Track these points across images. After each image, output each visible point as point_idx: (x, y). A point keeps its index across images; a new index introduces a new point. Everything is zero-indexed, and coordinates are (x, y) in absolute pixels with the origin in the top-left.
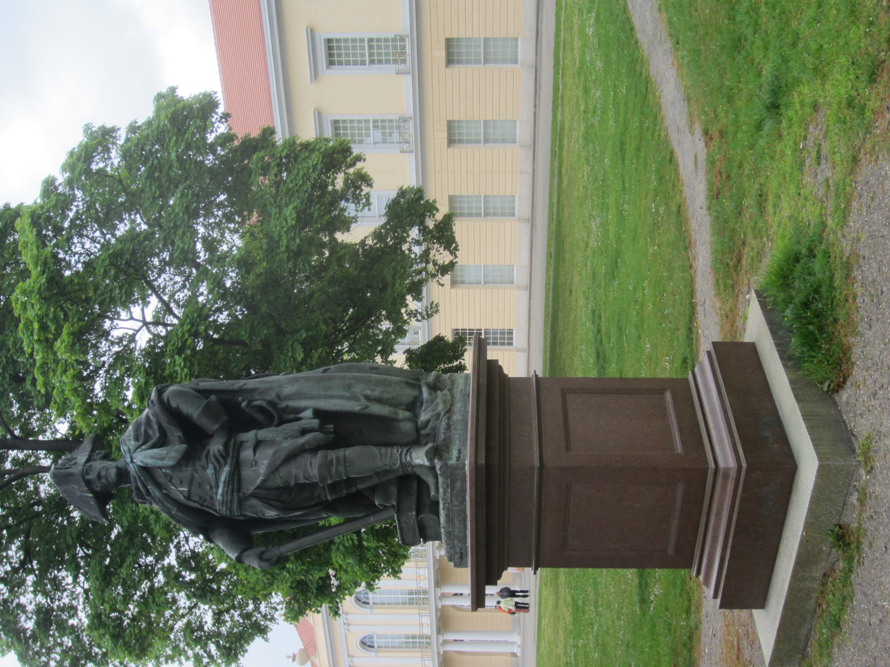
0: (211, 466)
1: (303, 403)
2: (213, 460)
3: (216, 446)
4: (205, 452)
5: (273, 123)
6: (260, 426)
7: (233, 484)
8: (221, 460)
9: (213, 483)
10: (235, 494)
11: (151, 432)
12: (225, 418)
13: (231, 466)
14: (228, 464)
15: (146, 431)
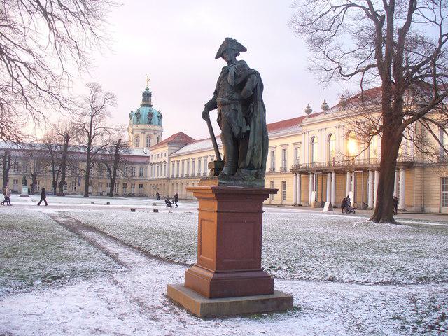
3: (235, 96)
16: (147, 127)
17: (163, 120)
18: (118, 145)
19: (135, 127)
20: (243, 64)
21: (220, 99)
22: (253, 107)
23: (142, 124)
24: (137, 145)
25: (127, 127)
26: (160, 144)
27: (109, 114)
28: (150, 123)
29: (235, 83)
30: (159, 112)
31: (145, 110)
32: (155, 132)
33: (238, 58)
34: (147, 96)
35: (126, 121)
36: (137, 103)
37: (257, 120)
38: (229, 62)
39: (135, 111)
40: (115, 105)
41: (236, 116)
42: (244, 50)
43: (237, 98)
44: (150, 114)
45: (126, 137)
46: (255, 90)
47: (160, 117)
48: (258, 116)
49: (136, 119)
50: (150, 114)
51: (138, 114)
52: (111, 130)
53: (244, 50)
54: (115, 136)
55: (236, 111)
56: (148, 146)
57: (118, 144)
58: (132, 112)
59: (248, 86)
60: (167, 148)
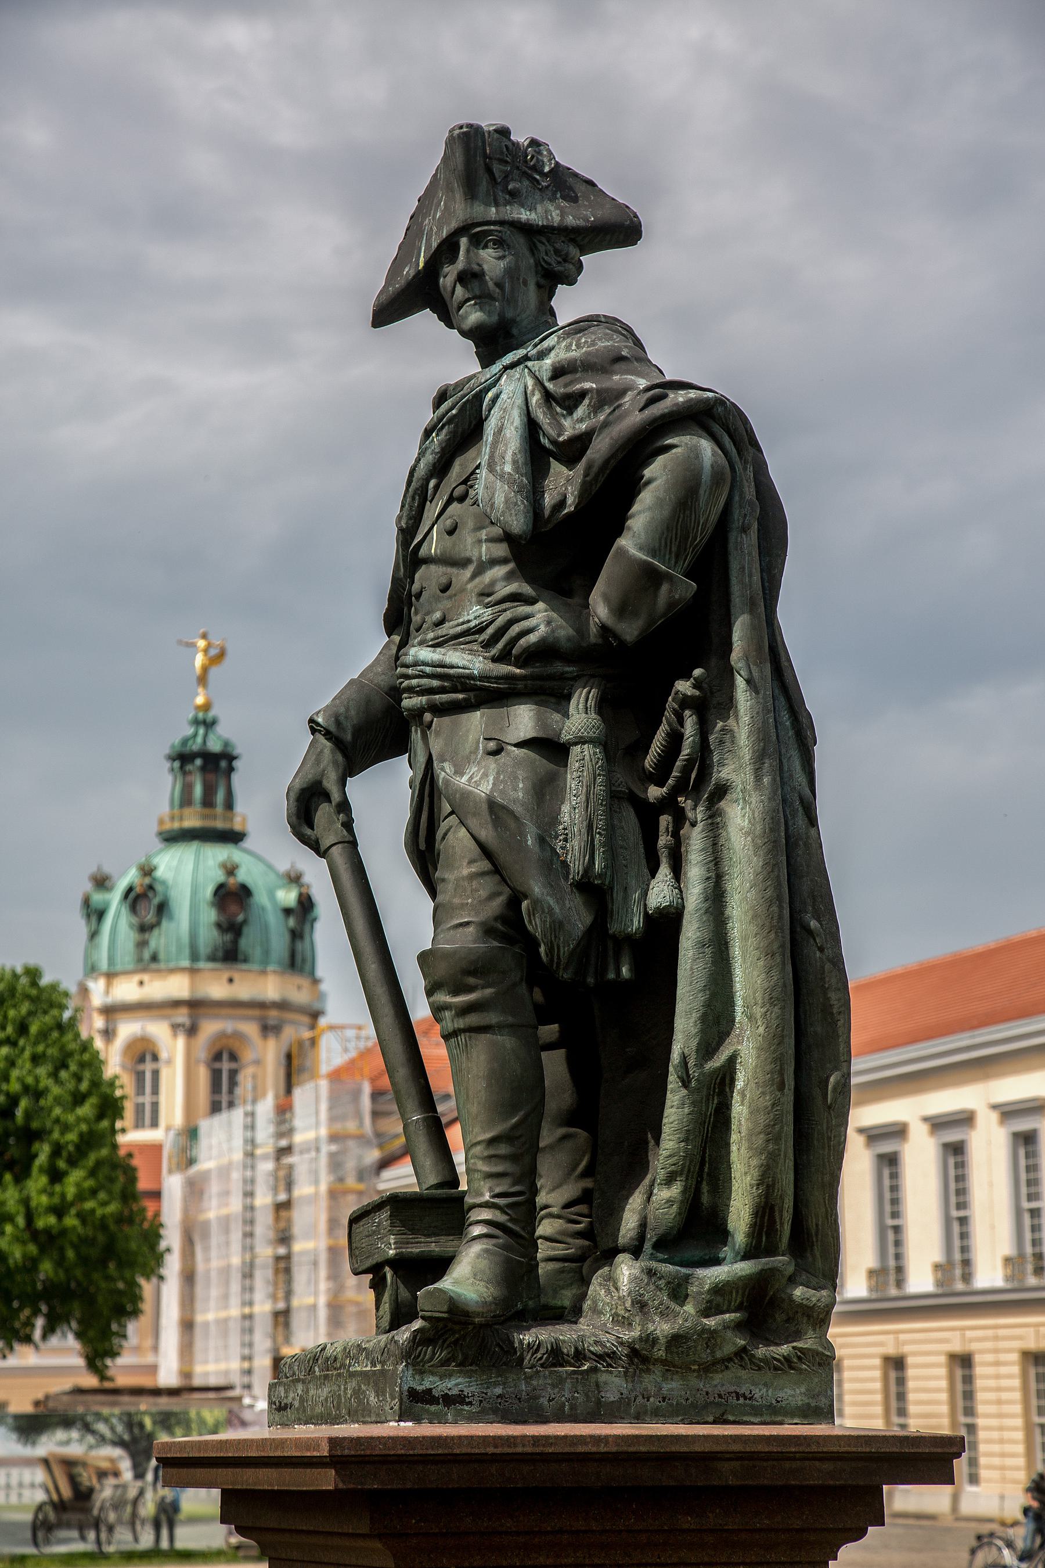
0: (487, 614)
1: (695, 872)
3: (540, 621)
4: (527, 589)
5: (119, 878)
7: (442, 690)
9: (449, 629)
10: (422, 700)
11: (580, 412)
12: (630, 631)
13: (483, 677)
14: (491, 665)
15: (583, 394)
28: (230, 955)
53: (623, 231)
58: (102, 882)
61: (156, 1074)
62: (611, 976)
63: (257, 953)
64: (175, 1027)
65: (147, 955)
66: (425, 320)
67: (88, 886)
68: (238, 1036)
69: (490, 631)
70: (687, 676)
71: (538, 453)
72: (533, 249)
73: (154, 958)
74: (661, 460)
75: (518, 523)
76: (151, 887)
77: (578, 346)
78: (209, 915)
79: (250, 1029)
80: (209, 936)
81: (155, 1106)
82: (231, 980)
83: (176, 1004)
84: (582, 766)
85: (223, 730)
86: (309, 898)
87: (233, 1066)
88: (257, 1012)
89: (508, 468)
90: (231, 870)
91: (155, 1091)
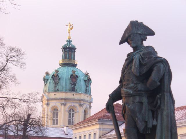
2: (135, 86)
3: (140, 87)
4: (138, 82)
6: (149, 103)
8: (135, 89)
16: (70, 95)
17: (93, 86)
18: (27, 122)
19: (52, 95)
20: (151, 51)
21: (124, 90)
22: (160, 99)
23: (62, 91)
24: (55, 122)
25: (39, 97)
26: (87, 121)
27: (13, 78)
28: (73, 90)
29: (140, 73)
30: (87, 75)
31: (67, 72)
32: (81, 102)
33: (146, 44)
34: (69, 51)
35: (38, 88)
36: (54, 62)
37: (165, 113)
38: (135, 48)
39: (51, 72)
40: (22, 65)
41: (141, 109)
42: (152, 33)
43: (143, 89)
44: (74, 78)
45: (39, 111)
46: (162, 80)
47: (88, 81)
48: (166, 108)
49: (52, 85)
50: (74, 78)
51: (56, 77)
52: (17, 101)
53: (152, 33)
54: (22, 109)
55: (141, 103)
56: (70, 122)
57: (27, 121)
58: (47, 74)
59: (154, 76)
60: (98, 126)
61: (57, 113)
62: (148, 133)
63: (78, 90)
64: (61, 104)
65: (56, 89)
66: (126, 43)
67: (45, 75)
68: (74, 106)
69: (134, 87)
70: (159, 94)
71: (141, 65)
72: (141, 37)
73: (58, 90)
74: (156, 67)
75: (138, 74)
76: (57, 75)
77: (146, 51)
78: (69, 82)
79: (77, 105)
80: (69, 86)
81: (57, 120)
82: (73, 95)
83: (62, 99)
84: (145, 105)
85: (72, 43)
86: (90, 78)
87: (73, 112)
88: (78, 102)
89: (136, 67)
90: (74, 72)
91: (57, 117)
